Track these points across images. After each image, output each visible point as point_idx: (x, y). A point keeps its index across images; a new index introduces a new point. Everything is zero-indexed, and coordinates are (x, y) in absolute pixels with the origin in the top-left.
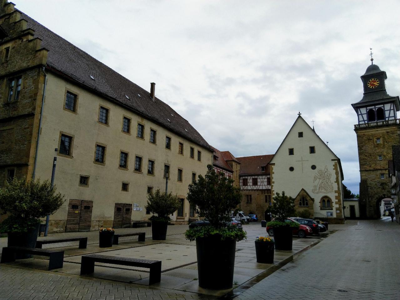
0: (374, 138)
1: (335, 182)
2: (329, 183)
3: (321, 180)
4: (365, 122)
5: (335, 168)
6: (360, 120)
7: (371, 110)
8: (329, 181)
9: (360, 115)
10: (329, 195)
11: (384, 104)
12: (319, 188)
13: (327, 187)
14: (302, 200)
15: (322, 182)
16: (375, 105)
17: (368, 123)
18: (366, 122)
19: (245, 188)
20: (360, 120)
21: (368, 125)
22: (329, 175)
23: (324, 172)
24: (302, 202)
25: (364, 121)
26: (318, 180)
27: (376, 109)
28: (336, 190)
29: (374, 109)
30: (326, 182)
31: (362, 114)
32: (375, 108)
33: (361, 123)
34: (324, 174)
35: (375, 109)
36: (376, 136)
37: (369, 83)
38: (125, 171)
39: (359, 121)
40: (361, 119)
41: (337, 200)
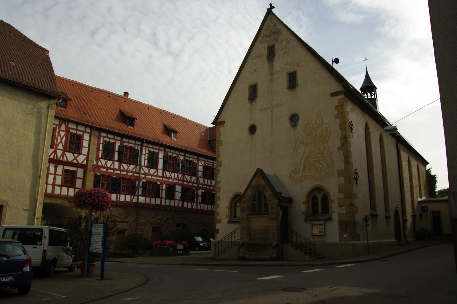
23: (315, 126)
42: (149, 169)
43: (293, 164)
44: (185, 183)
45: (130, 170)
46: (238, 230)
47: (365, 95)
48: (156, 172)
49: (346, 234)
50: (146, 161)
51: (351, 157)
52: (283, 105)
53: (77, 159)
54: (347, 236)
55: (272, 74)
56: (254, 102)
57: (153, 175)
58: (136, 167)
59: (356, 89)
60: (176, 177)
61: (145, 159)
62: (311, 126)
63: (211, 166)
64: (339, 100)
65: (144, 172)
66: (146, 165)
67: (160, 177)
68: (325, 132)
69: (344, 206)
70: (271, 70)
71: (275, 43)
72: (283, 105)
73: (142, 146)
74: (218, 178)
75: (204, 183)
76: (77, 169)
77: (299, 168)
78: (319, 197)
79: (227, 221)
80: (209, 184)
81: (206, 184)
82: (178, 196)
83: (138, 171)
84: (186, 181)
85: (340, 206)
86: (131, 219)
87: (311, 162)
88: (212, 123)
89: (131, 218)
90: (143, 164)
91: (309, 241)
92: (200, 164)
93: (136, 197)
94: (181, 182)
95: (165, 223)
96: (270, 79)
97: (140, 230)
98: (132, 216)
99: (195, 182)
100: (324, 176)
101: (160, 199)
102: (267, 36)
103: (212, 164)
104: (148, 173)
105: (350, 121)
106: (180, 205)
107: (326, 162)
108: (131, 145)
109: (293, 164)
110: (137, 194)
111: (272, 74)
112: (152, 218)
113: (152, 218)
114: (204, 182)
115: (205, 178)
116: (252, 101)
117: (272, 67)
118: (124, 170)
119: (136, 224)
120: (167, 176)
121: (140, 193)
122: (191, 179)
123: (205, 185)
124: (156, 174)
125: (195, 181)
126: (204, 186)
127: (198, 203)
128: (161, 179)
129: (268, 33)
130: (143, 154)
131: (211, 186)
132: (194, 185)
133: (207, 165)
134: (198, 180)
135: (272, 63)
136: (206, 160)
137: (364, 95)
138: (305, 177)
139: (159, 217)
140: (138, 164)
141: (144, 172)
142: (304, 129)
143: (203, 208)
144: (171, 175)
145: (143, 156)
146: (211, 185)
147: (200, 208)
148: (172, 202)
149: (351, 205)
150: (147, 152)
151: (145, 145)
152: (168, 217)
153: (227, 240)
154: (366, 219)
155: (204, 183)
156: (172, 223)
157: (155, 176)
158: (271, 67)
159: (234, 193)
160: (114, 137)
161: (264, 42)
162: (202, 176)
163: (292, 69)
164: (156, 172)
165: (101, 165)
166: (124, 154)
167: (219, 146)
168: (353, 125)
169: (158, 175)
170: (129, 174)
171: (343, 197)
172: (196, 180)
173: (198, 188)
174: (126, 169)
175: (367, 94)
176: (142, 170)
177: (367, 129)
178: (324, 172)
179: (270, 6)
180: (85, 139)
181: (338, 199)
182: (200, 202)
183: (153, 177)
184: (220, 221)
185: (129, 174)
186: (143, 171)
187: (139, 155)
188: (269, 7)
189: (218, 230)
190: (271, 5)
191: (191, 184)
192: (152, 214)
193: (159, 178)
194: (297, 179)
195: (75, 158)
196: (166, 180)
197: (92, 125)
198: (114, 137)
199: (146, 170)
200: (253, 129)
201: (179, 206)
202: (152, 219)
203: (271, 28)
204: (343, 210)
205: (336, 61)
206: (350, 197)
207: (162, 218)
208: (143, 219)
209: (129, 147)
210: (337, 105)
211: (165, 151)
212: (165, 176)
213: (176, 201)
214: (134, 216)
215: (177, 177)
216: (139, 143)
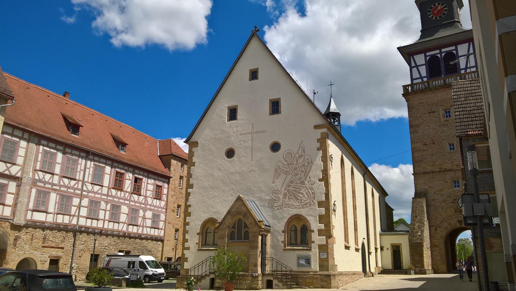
0: (441, 110)
1: (320, 180)
2: (306, 182)
3: (289, 177)
4: (422, 80)
5: (321, 146)
6: (414, 77)
7: (434, 58)
8: (306, 179)
9: (414, 67)
10: (303, 212)
11: (456, 44)
13: (302, 194)
14: (236, 226)
15: (292, 182)
16: (440, 48)
17: (428, 82)
18: (425, 79)
20: (414, 77)
21: (428, 84)
22: (306, 164)
23: (297, 156)
24: (236, 231)
25: (421, 77)
27: (443, 54)
28: (320, 200)
29: (439, 55)
30: (298, 182)
31: (417, 66)
32: (441, 53)
33: (415, 82)
34: (297, 161)
35: (441, 55)
36: (444, 105)
37: (429, 12)
39: (412, 79)
40: (416, 75)
41: (322, 226)
42: (70, 180)
43: (273, 192)
44: (131, 203)
45: (72, 186)
46: (210, 258)
48: (101, 190)
50: (90, 176)
53: (10, 169)
57: (96, 193)
61: (89, 174)
62: (293, 156)
64: (322, 134)
65: (87, 188)
66: (90, 181)
67: (104, 195)
75: (152, 204)
76: (8, 183)
80: (157, 205)
81: (155, 204)
82: (123, 218)
83: (80, 187)
86: (67, 245)
87: (292, 191)
88: (184, 141)
90: (86, 180)
94: (128, 202)
97: (77, 258)
100: (304, 205)
105: (330, 154)
109: (273, 192)
112: (92, 243)
113: (92, 243)
114: (152, 202)
118: (65, 186)
120: (113, 195)
122: (138, 199)
123: (153, 206)
124: (100, 192)
125: (143, 202)
130: (88, 168)
134: (146, 201)
139: (100, 242)
143: (149, 233)
144: (116, 194)
146: (160, 206)
150: (92, 166)
152: (110, 242)
155: (152, 204)
157: (99, 194)
160: (56, 146)
164: (101, 190)
168: (332, 157)
174: (66, 184)
179: (255, 29)
180: (21, 146)
183: (97, 196)
190: (256, 27)
193: (103, 197)
194: (276, 207)
195: (8, 169)
196: (111, 199)
197: (31, 130)
198: (56, 146)
199: (90, 187)
201: (123, 230)
212: (110, 194)
214: (71, 241)
215: (123, 196)
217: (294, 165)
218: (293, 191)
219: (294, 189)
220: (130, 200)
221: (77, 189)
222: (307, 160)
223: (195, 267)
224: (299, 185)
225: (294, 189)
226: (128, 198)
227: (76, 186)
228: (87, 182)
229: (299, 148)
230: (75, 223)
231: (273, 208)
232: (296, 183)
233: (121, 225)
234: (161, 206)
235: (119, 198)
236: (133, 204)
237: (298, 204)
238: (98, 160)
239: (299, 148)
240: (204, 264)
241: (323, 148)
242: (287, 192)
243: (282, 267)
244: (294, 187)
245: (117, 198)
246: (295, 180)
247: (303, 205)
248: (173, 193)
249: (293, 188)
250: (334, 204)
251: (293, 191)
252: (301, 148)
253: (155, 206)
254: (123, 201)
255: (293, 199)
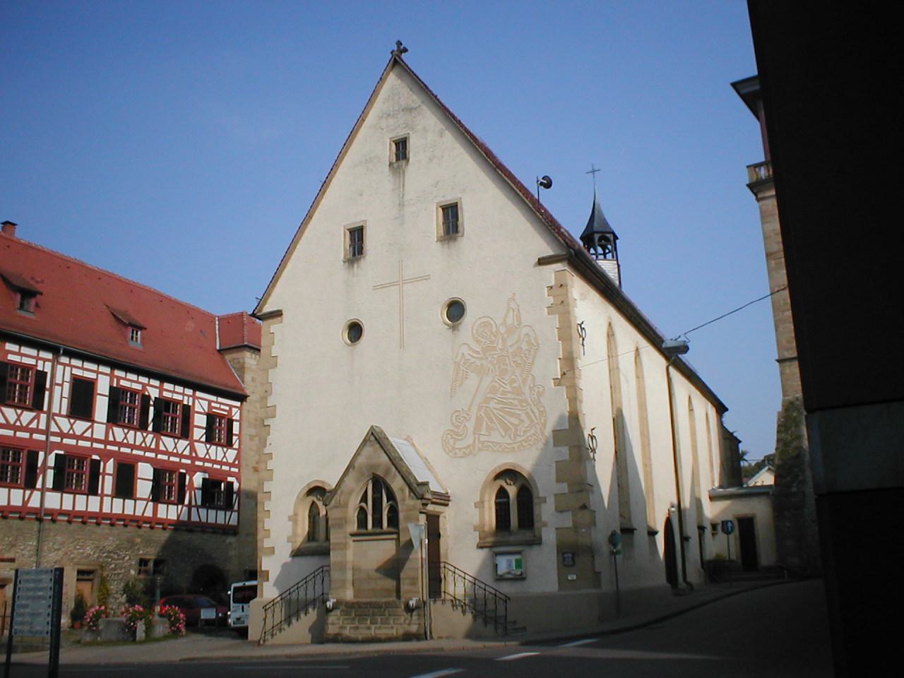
2: (526, 390)
12: (479, 420)
19: (22, 313)
22: (524, 346)
23: (502, 330)
26: (472, 381)
30: (508, 388)
34: (504, 340)
38: (535, 478)
43: (452, 417)
47: (592, 251)
49: (574, 574)
51: (581, 402)
52: (427, 278)
54: (575, 577)
55: (402, 205)
56: (358, 267)
57: (81, 437)
58: (37, 417)
59: (574, 237)
60: (138, 443)
62: (494, 330)
63: (226, 413)
66: (64, 412)
68: (524, 343)
69: (568, 511)
70: (399, 195)
71: (409, 134)
72: (427, 278)
73: (55, 362)
74: (265, 447)
77: (465, 426)
78: (512, 491)
79: (290, 551)
80: (219, 459)
82: (144, 488)
83: (43, 426)
84: (164, 451)
85: (560, 510)
86: (23, 552)
87: (494, 410)
89: (22, 550)
90: (55, 410)
91: (493, 592)
92: (198, 408)
93: (37, 495)
94: (152, 455)
95: (110, 560)
96: (397, 216)
98: (24, 544)
99: (184, 453)
100: (523, 443)
101: (99, 498)
102: (389, 115)
103: (227, 408)
104: (15, 422)
106: (149, 513)
107: (528, 412)
108: (26, 361)
109: (452, 417)
110: (39, 485)
111: (402, 205)
112: (78, 547)
115: (212, 444)
116: (353, 267)
117: (401, 190)
119: (35, 565)
121: (50, 484)
123: (210, 461)
124: (88, 434)
125: (187, 452)
126: (207, 465)
127: (194, 506)
128: (102, 446)
129: (391, 109)
130: (58, 385)
131: (207, 459)
132: (184, 461)
133: (214, 410)
134: (193, 449)
135: (402, 180)
136: (213, 398)
137: (589, 251)
138: (480, 446)
140: (45, 408)
141: (58, 431)
142: (477, 336)
143: (204, 520)
145: (57, 389)
146: (224, 460)
147: (198, 520)
148: (129, 503)
149: (584, 507)
150: (68, 378)
151: (64, 360)
152: (118, 542)
153: (294, 596)
154: (612, 539)
156: (127, 558)
157: (87, 439)
158: (400, 188)
159: (306, 484)
161: (382, 129)
162: (204, 439)
163: (449, 199)
165: (113, 440)
166: (8, 384)
167: (270, 371)
169: (94, 437)
170: (19, 434)
171: (567, 491)
172: (189, 447)
173: (193, 469)
174: (12, 422)
175: (595, 250)
176: (53, 424)
177: (611, 335)
178: (522, 434)
179: (398, 47)
181: (555, 495)
182: (199, 503)
183: (81, 443)
184: (272, 551)
185: (19, 434)
186: (56, 427)
187: (48, 386)
188: (395, 48)
189: (267, 572)
190: (399, 43)
191: (177, 460)
192: (79, 537)
193: (96, 445)
194: (460, 449)
196: (116, 448)
199: (64, 424)
200: (355, 331)
202: (78, 549)
203: (400, 98)
204: (567, 521)
205: (545, 182)
206: (581, 491)
207: (104, 547)
208: (55, 550)
209: (20, 366)
210: (553, 283)
211: (112, 376)
212: (111, 439)
213: (110, 498)
216: (49, 356)
217: (496, 350)
218: (497, 409)
219: (498, 406)
220: (157, 451)
221: (38, 431)
222: (527, 339)
223: (292, 590)
224: (509, 395)
225: (498, 406)
226: (153, 446)
227: (33, 425)
228: (60, 415)
229: (508, 311)
230: (38, 505)
231: (454, 452)
232: (504, 393)
233: (141, 504)
234: (73, 431)
235: (133, 447)
236: (165, 457)
237: (509, 441)
238: (80, 366)
239: (508, 311)
240: (310, 582)
241: (562, 307)
242: (484, 413)
243: (456, 576)
244: (499, 402)
245: (127, 446)
246: (500, 385)
247: (520, 442)
248: (253, 431)
249: (496, 403)
250: (592, 437)
251: (497, 409)
252: (511, 311)
253: (215, 462)
254: (141, 453)
255: (497, 429)
